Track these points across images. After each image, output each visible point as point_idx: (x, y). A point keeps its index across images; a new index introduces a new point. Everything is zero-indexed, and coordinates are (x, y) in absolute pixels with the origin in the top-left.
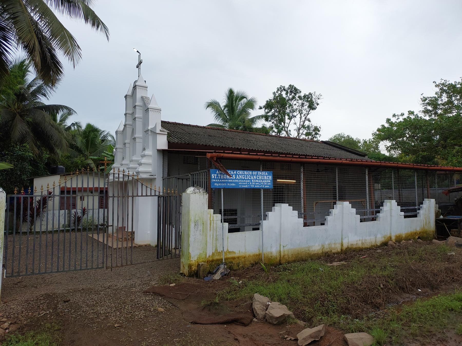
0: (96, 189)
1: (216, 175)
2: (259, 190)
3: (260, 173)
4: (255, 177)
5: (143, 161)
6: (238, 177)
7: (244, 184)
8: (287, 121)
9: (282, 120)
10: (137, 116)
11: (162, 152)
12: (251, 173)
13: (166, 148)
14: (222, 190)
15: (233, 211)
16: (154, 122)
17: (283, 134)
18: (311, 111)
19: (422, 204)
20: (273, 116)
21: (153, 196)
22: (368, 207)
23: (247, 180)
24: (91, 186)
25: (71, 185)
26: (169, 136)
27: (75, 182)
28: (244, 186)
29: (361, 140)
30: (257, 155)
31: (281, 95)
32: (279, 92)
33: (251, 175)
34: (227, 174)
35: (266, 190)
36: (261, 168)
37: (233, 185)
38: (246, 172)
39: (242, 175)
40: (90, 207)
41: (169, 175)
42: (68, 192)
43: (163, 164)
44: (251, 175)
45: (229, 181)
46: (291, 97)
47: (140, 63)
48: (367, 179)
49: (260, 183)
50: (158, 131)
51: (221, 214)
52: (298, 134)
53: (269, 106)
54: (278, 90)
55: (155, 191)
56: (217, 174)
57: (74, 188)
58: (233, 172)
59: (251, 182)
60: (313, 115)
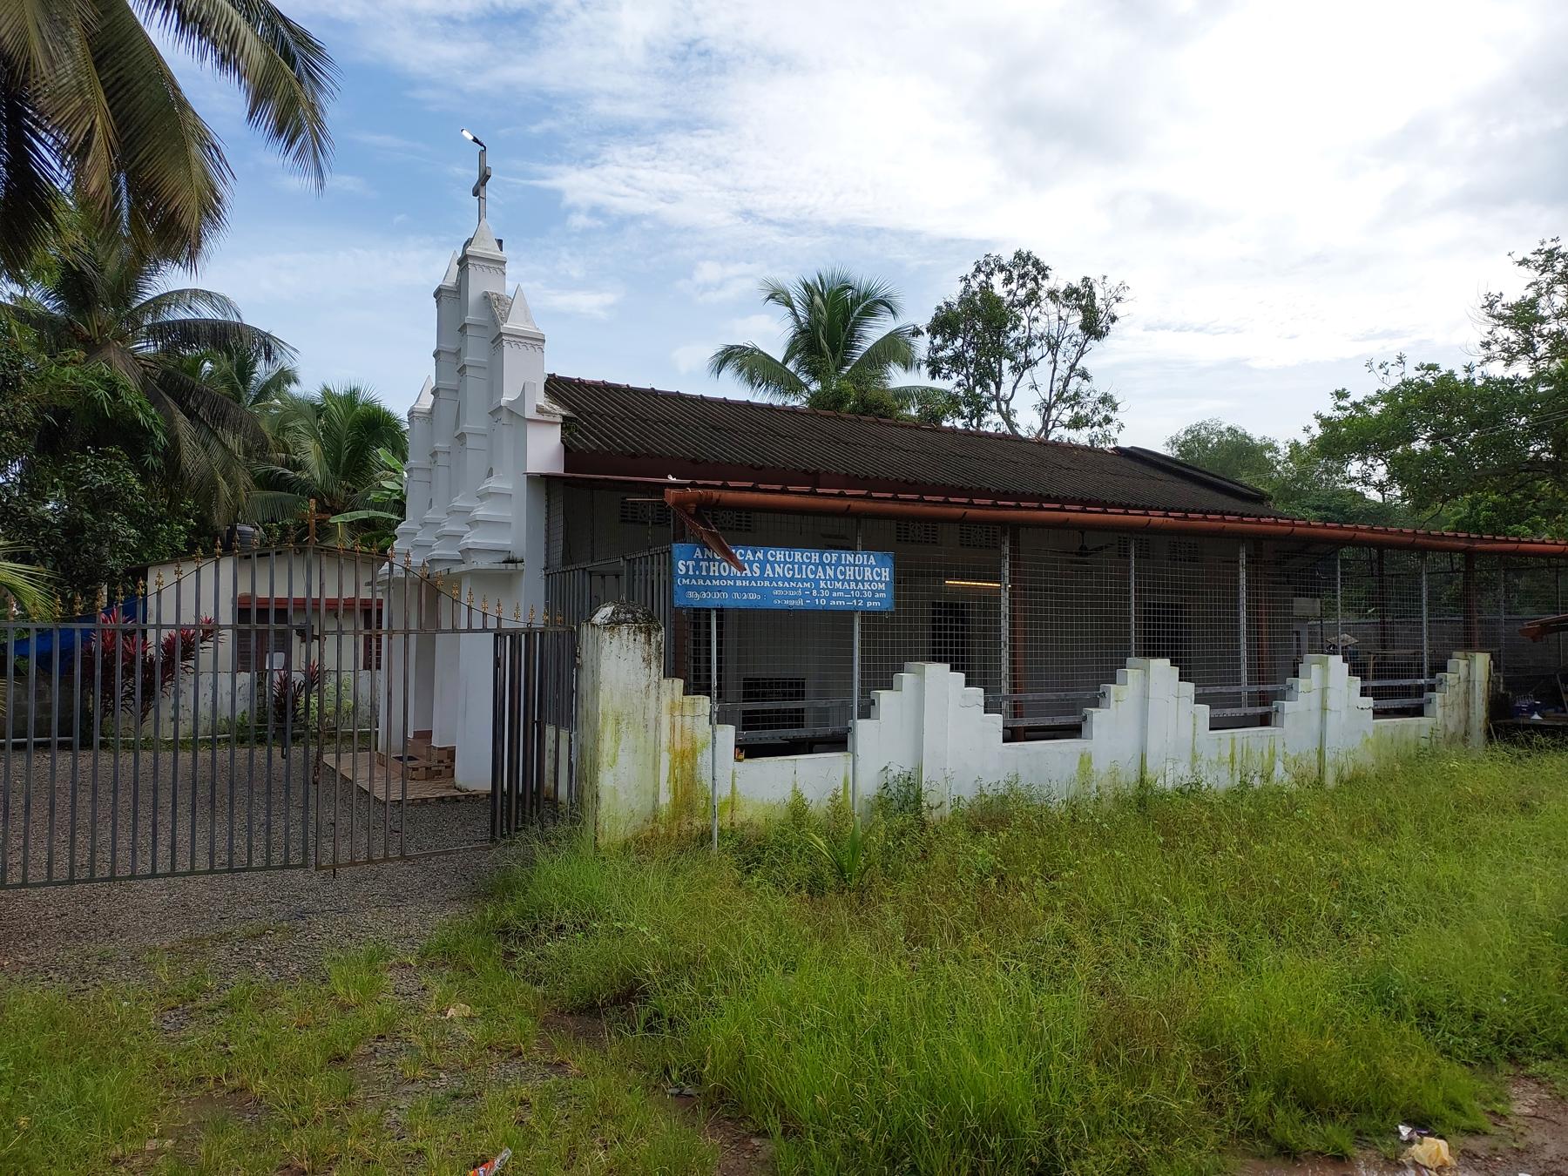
0: (349, 604)
1: (690, 563)
2: (845, 616)
3: (849, 557)
4: (830, 572)
5: (480, 511)
6: (769, 572)
7: (792, 593)
8: (1008, 378)
9: (987, 374)
10: (468, 359)
11: (544, 482)
12: (815, 557)
13: (558, 469)
14: (714, 614)
15: (791, 685)
16: (521, 380)
17: (992, 423)
18: (1092, 342)
19: (1444, 669)
20: (957, 361)
21: (476, 631)
22: (1244, 679)
23: (803, 581)
24: (331, 593)
25: (290, 593)
26: (567, 424)
27: (281, 582)
28: (792, 603)
29: (1280, 445)
30: (841, 495)
31: (986, 288)
32: (982, 277)
33: (816, 565)
34: (731, 558)
35: (870, 617)
36: (859, 541)
37: (753, 596)
38: (798, 555)
39: (785, 563)
40: (330, 662)
41: (568, 558)
42: (263, 614)
43: (548, 525)
44: (816, 565)
45: (739, 583)
46: (1022, 293)
47: (484, 178)
48: (1243, 582)
49: (848, 591)
50: (530, 413)
51: (709, 694)
52: (1045, 423)
53: (944, 324)
54: (978, 270)
55: (485, 614)
56: (698, 561)
57: (279, 601)
58: (754, 553)
59: (818, 588)
60: (1098, 358)
